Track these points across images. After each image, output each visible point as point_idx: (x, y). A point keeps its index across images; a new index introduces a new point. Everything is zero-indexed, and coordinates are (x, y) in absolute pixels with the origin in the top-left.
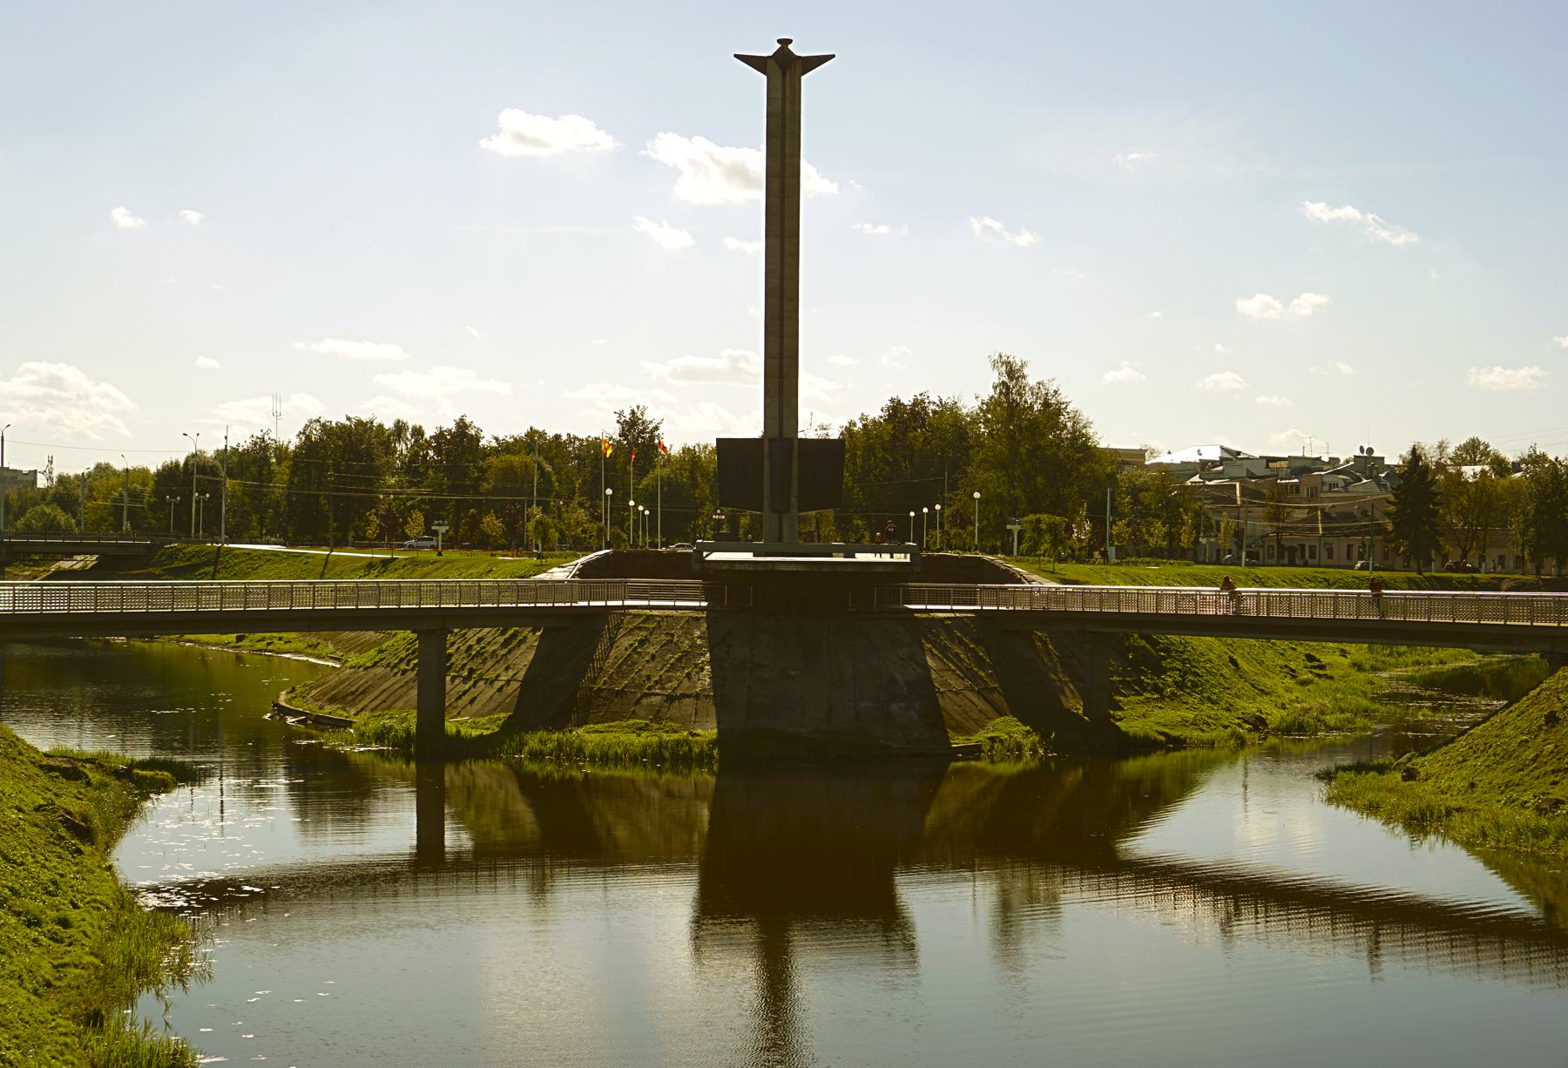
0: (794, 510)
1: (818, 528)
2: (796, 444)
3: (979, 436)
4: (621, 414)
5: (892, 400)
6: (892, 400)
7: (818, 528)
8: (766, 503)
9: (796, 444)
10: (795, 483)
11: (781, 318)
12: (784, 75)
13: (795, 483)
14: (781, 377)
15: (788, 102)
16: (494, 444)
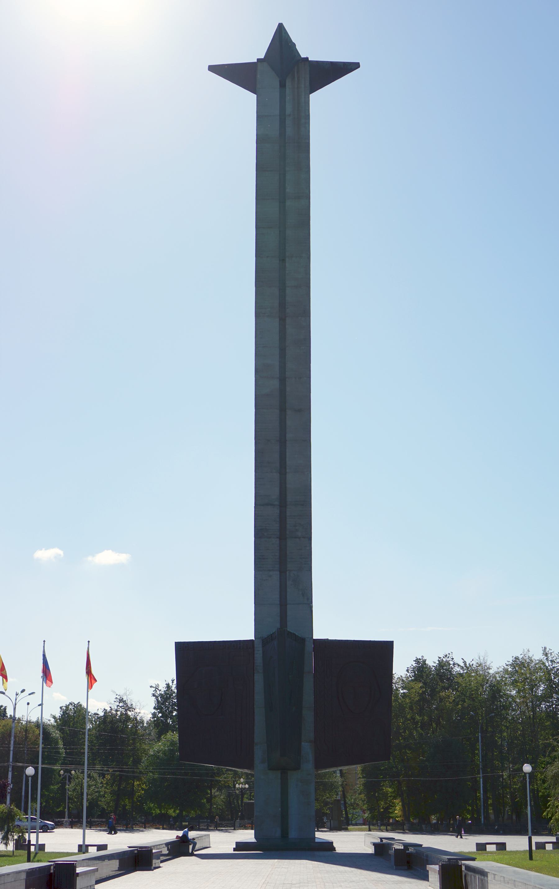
0: (308, 766)
1: (344, 796)
2: (309, 647)
3: (516, 693)
4: (156, 688)
5: (417, 661)
6: (417, 661)
7: (344, 796)
8: (259, 752)
9: (309, 647)
10: (309, 717)
11: (283, 442)
12: (283, 85)
13: (309, 717)
14: (283, 537)
15: (289, 122)
16: (52, 721)
